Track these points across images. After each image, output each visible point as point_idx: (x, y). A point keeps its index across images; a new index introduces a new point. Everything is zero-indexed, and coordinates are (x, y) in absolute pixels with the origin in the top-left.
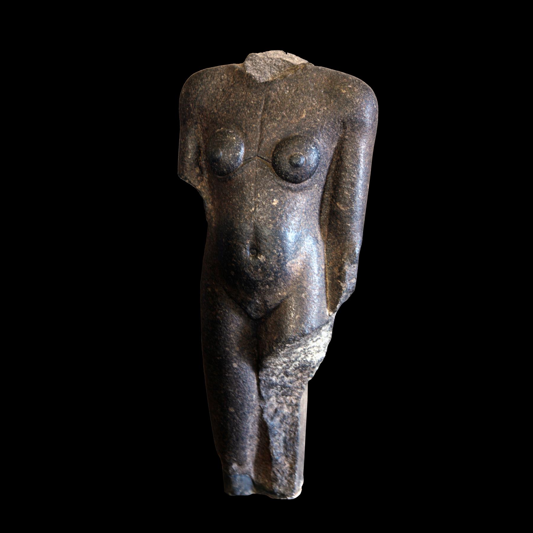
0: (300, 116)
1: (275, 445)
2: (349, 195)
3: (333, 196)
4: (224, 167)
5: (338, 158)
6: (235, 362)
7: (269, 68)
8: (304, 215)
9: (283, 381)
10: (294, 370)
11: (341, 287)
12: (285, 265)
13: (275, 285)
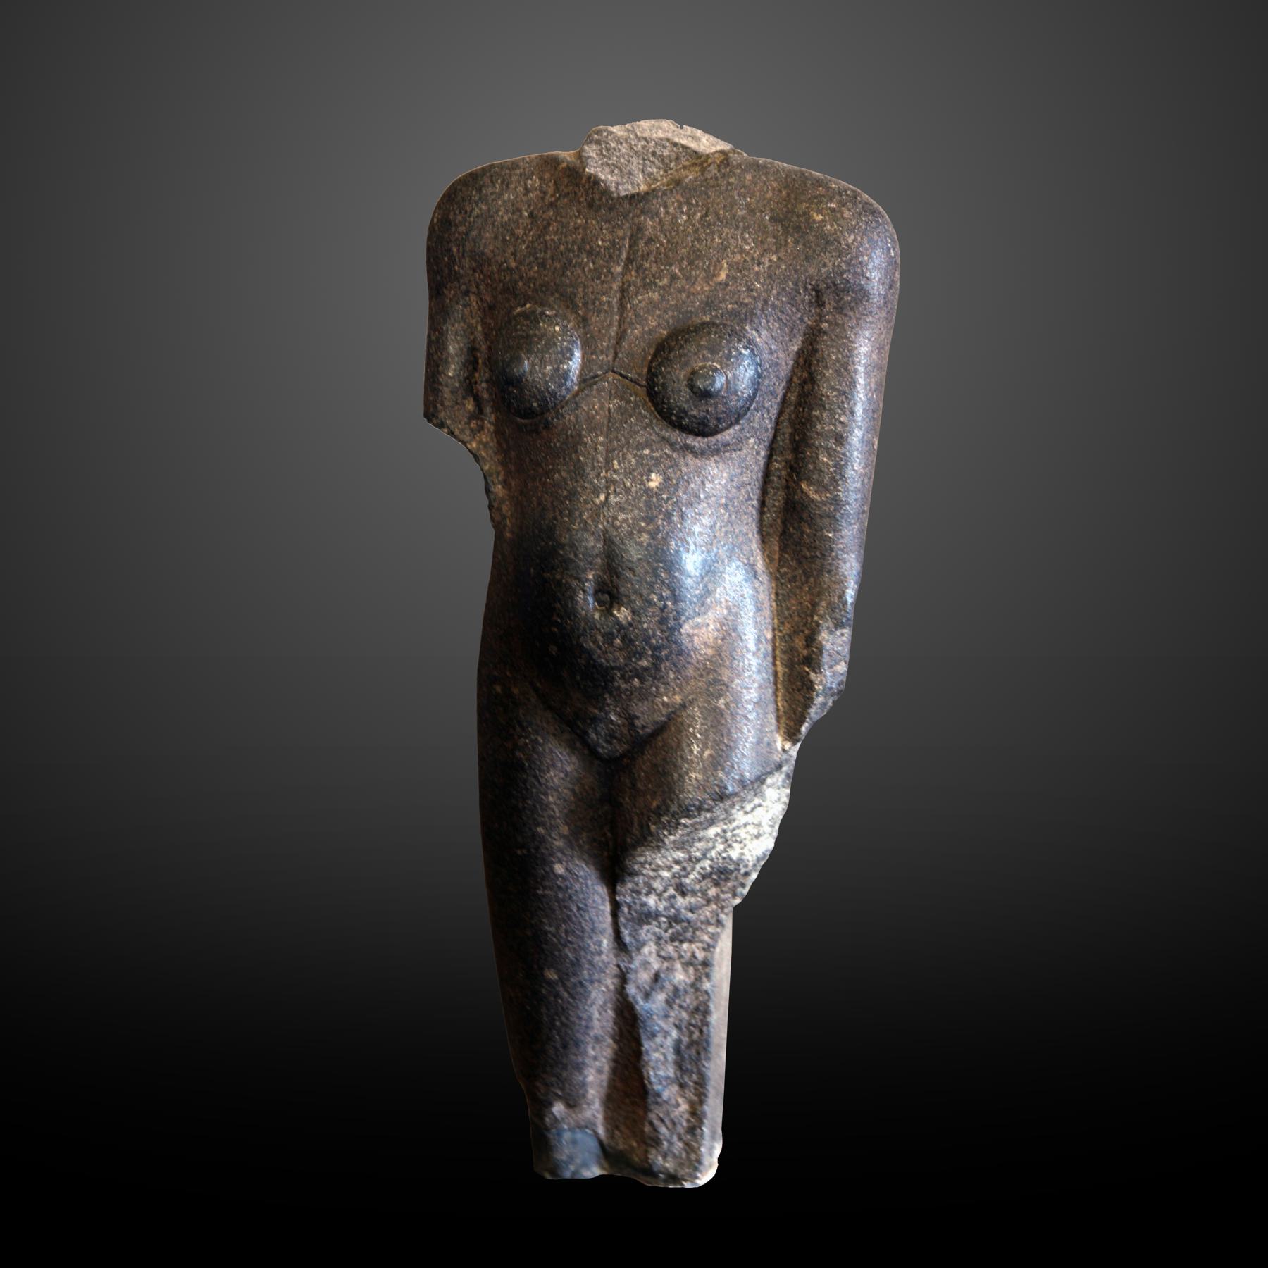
0: (714, 275)
1: (653, 1058)
2: (831, 463)
3: (791, 467)
4: (533, 397)
5: (805, 375)
6: (560, 862)
7: (641, 162)
8: (723, 511)
9: (672, 906)
11: (811, 682)
12: (679, 631)
13: (655, 678)
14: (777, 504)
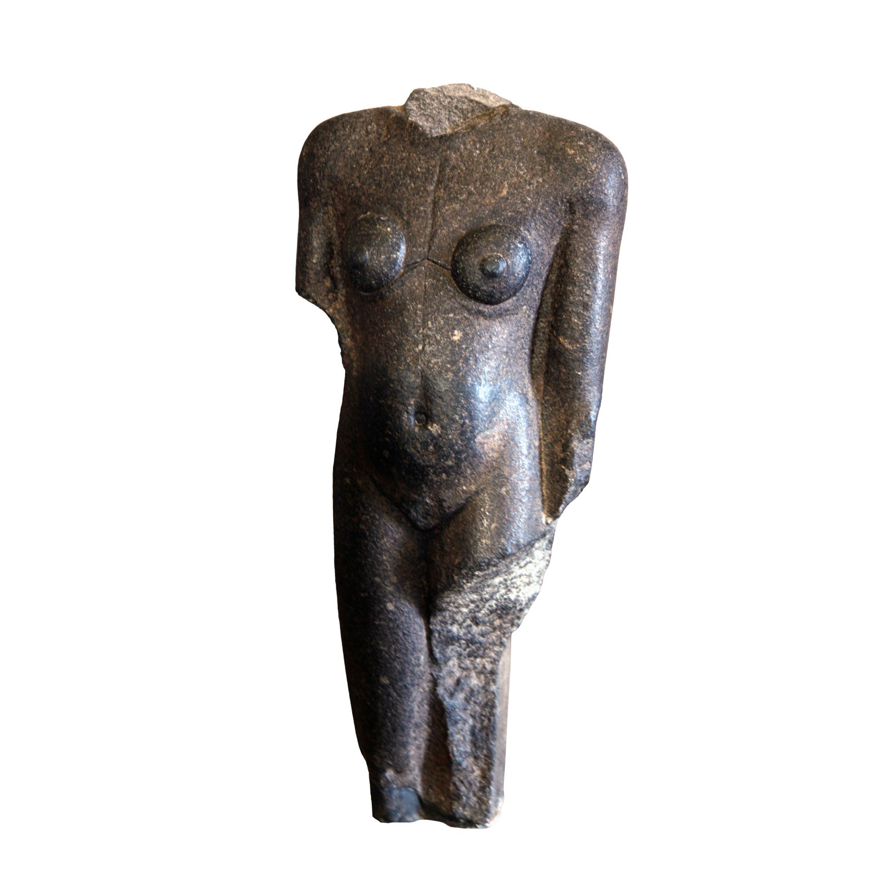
0: (498, 192)
1: (456, 739)
2: (580, 323)
3: (552, 326)
4: (372, 277)
5: (562, 262)
6: (391, 601)
7: (447, 113)
9: (469, 632)
11: (566, 476)
13: (457, 473)
14: (542, 352)
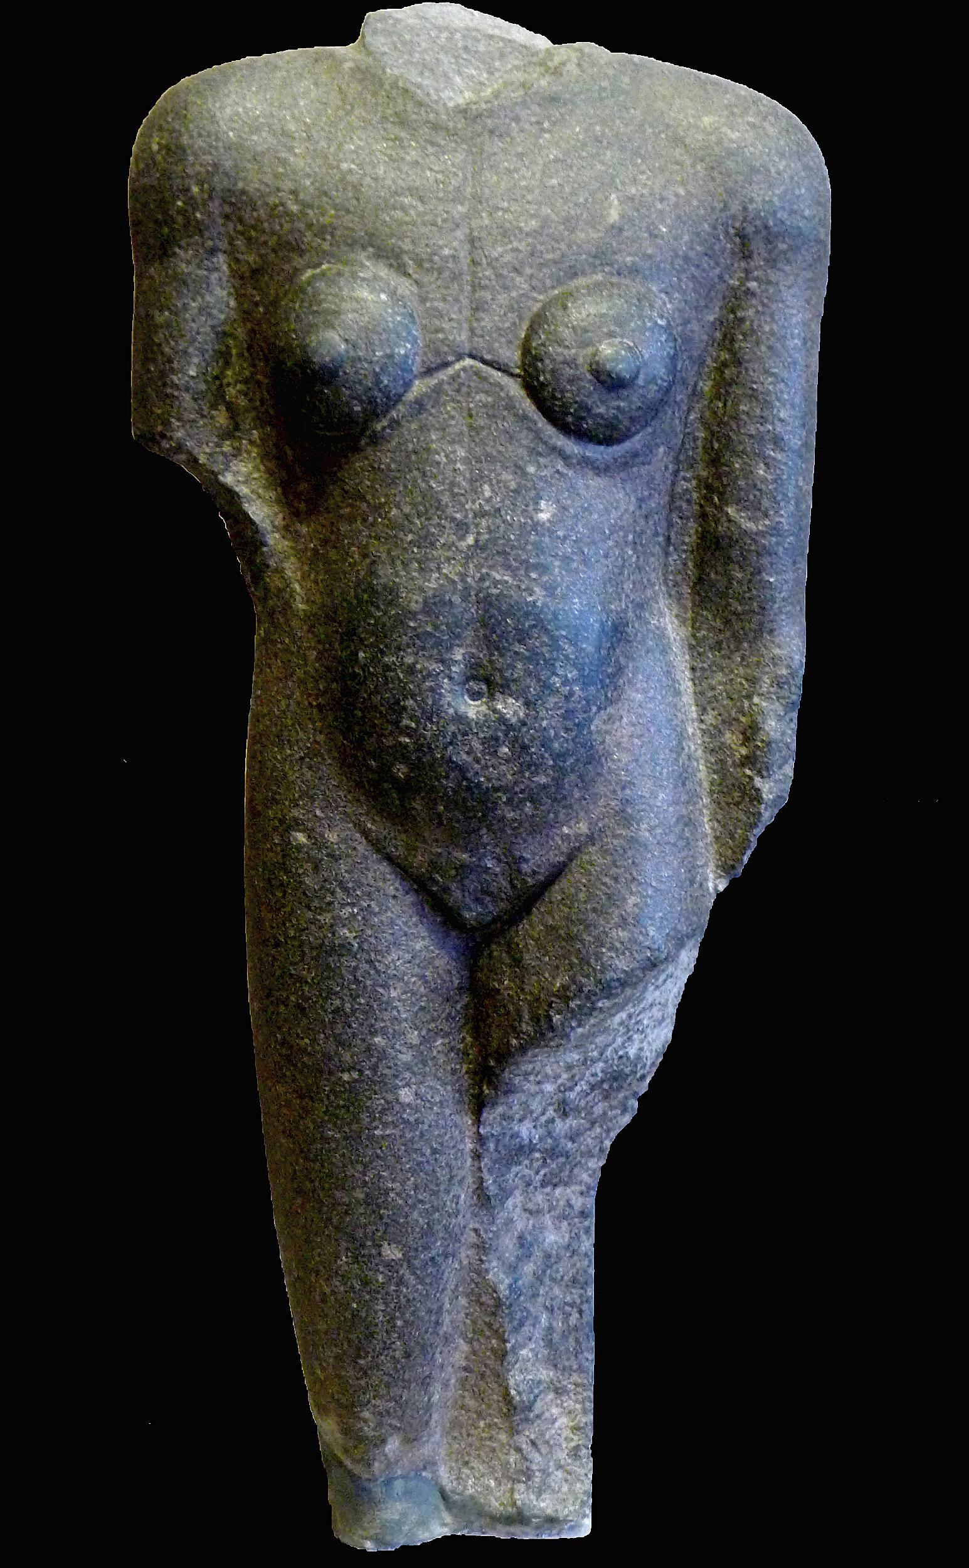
2: (769, 477)
3: (708, 487)
4: (355, 399)
5: (725, 356)
7: (453, 61)
9: (550, 1134)
10: (588, 1094)
11: (758, 790)
13: (555, 800)
14: (687, 540)
